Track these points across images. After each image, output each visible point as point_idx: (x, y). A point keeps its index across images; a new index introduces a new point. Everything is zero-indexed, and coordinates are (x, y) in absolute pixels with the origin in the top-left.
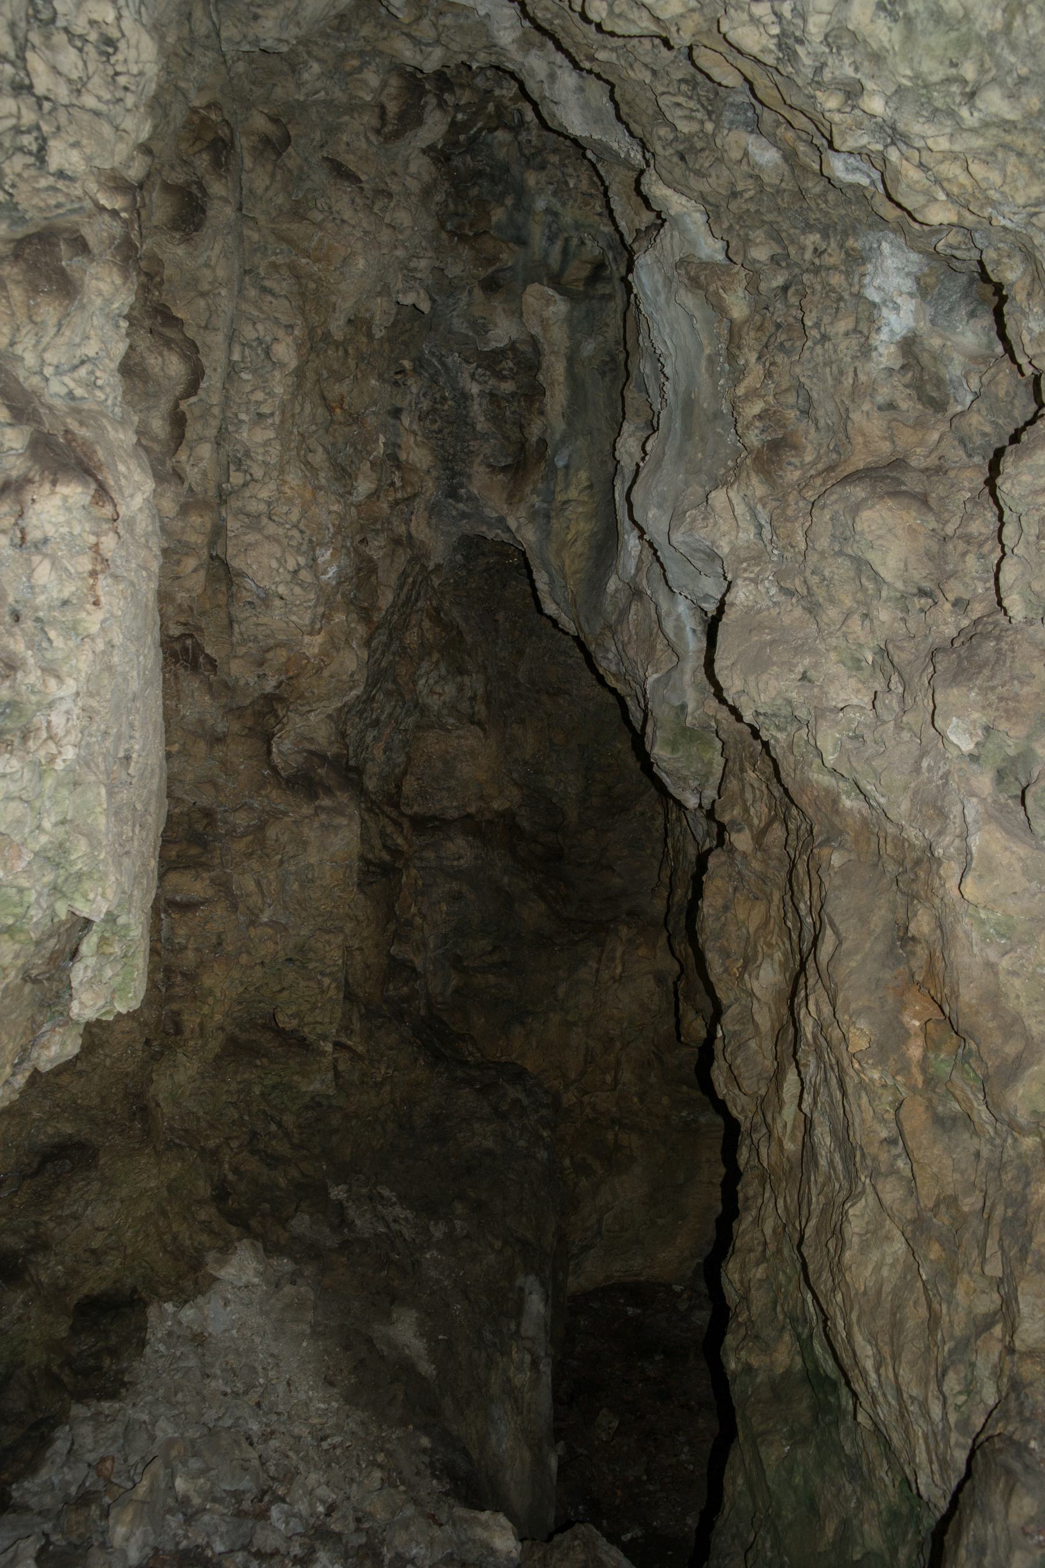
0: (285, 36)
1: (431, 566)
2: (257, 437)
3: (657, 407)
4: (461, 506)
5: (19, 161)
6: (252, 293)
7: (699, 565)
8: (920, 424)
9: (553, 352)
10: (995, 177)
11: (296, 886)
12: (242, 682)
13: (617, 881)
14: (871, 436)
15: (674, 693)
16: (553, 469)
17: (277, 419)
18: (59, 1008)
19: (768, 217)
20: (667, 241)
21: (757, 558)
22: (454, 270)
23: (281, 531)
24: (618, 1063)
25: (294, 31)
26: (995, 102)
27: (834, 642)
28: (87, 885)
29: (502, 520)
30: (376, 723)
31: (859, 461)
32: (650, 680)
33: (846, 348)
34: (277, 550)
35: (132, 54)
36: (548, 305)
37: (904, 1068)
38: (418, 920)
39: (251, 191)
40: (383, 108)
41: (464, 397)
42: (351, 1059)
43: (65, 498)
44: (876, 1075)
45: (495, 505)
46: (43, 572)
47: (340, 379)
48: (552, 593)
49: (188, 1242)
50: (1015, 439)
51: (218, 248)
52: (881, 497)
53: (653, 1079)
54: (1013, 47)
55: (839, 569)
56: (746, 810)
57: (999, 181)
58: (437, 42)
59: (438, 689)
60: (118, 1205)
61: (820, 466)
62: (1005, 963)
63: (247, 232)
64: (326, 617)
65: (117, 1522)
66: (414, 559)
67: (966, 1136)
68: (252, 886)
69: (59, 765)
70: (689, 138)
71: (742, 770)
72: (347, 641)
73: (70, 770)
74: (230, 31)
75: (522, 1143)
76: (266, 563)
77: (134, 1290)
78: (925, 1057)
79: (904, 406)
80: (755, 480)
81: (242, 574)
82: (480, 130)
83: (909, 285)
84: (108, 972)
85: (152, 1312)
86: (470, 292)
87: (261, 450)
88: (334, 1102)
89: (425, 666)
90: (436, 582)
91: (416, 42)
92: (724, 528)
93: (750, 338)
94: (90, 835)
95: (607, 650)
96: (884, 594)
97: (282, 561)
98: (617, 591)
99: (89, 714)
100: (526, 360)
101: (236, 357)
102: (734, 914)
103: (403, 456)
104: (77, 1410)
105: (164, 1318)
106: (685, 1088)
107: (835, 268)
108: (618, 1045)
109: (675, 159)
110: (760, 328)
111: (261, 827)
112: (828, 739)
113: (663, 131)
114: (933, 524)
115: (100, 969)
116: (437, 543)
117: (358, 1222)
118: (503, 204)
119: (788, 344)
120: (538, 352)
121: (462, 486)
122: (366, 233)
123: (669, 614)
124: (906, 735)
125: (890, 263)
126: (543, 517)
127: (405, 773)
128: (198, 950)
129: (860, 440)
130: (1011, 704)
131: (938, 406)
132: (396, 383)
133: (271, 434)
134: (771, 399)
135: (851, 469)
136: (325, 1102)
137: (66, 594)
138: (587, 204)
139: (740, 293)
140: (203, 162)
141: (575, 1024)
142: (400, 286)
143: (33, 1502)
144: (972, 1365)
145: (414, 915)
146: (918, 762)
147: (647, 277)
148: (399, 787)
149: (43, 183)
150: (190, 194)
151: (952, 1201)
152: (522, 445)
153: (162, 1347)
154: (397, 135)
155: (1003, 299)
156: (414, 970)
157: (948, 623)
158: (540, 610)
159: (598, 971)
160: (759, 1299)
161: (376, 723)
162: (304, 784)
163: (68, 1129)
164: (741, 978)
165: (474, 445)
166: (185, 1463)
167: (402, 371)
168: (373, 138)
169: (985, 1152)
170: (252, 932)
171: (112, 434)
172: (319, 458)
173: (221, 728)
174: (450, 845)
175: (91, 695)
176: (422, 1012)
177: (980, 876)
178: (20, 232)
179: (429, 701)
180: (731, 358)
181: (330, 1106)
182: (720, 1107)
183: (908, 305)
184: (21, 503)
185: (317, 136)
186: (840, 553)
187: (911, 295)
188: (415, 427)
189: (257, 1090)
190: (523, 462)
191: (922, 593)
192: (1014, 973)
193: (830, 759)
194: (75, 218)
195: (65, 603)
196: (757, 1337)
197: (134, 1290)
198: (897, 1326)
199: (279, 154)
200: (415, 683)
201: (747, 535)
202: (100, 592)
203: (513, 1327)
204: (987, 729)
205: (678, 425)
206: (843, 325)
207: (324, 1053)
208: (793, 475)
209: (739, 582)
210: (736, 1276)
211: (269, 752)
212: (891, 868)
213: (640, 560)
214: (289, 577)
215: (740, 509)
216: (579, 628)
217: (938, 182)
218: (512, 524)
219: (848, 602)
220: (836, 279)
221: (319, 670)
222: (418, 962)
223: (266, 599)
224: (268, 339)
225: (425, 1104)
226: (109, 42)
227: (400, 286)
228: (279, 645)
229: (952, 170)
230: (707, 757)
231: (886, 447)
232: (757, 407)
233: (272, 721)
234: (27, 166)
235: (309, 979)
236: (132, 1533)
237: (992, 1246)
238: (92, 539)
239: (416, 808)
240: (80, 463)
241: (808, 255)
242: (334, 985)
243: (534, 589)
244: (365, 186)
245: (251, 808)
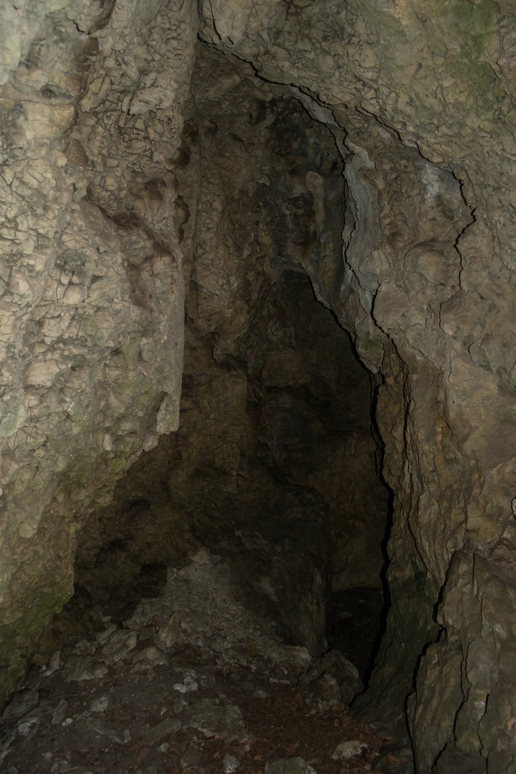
0: (217, 96)
1: (272, 283)
2: (208, 236)
3: (355, 220)
4: (283, 259)
5: (145, 159)
6: (205, 184)
7: (370, 278)
8: (444, 225)
9: (318, 198)
10: (450, 150)
11: (223, 406)
12: (202, 328)
14: (426, 230)
15: (364, 327)
16: (320, 244)
17: (215, 229)
18: (152, 429)
19: (388, 155)
20: (355, 161)
21: (389, 275)
22: (279, 168)
23: (217, 270)
25: (220, 94)
26: (444, 129)
27: (413, 302)
28: (167, 381)
29: (300, 264)
30: (251, 347)
31: (422, 239)
32: (357, 323)
33: (417, 200)
34: (215, 277)
35: (176, 122)
36: (315, 179)
37: (435, 444)
38: (269, 427)
39: (204, 148)
40: (251, 115)
41: (284, 216)
43: (164, 261)
44: (427, 448)
45: (297, 258)
46: (158, 283)
47: (237, 213)
48: (320, 292)
49: (181, 546)
50: (463, 232)
51: (194, 170)
52: (426, 252)
54: (447, 116)
55: (414, 277)
56: (391, 369)
57: (451, 151)
58: (271, 91)
59: (276, 333)
60: (157, 526)
61: (409, 241)
62: (464, 404)
63: (203, 162)
64: (233, 302)
65: (162, 633)
66: (265, 281)
67: (456, 465)
68: (207, 405)
69: (162, 341)
70: (360, 128)
71: (390, 354)
72: (241, 312)
73: (164, 343)
74: (198, 96)
75: (312, 516)
76: (210, 283)
77: (162, 562)
78: (442, 440)
79: (438, 219)
80: (387, 247)
81: (202, 287)
82: (287, 114)
83: (436, 178)
84: (168, 417)
85: (169, 570)
86: (285, 176)
87: (209, 241)
89: (270, 324)
90: (274, 290)
91: (263, 92)
92: (378, 264)
93: (385, 196)
94: (170, 364)
95: (342, 314)
96: (429, 285)
97: (217, 282)
98: (345, 290)
99: (170, 326)
100: (308, 201)
101: (200, 208)
102: (388, 408)
103: (260, 240)
104: (144, 600)
105: (172, 574)
107: (411, 172)
108: (354, 484)
109: (356, 135)
110: (388, 192)
111: (210, 381)
112: (410, 336)
113: (350, 126)
114: (444, 261)
115: (165, 415)
116: (274, 273)
117: (247, 544)
118: (297, 141)
119: (397, 198)
120: (312, 197)
121: (284, 251)
122: (246, 160)
123: (362, 298)
124: (435, 332)
125: (429, 171)
126: (316, 263)
127: (263, 367)
128: (187, 428)
129: (422, 232)
130: (464, 319)
131: (451, 218)
132: (257, 212)
133: (213, 235)
134: (392, 218)
135: (418, 242)
137: (164, 290)
138: (329, 140)
139: (382, 180)
140: (188, 140)
142: (258, 176)
143: (131, 627)
144: (456, 538)
146: (437, 340)
147: (350, 173)
148: (261, 373)
149: (152, 165)
150: (185, 152)
151: (451, 486)
152: (307, 233)
153: (173, 583)
154: (256, 123)
155: (462, 185)
156: (268, 446)
157: (449, 293)
158: (316, 299)
159: (344, 451)
160: (399, 552)
161: (251, 347)
162: (226, 365)
163: (140, 494)
164: (391, 432)
165: (288, 235)
166: (184, 619)
167: (259, 207)
168: (248, 125)
169: (461, 470)
170: (207, 421)
171: (173, 241)
172: (230, 243)
173: (195, 345)
175: (170, 321)
176: (271, 465)
177: (455, 375)
178: (146, 180)
180: (379, 203)
182: (386, 485)
183: (436, 185)
184: (152, 263)
185: (227, 126)
186: (414, 272)
187: (437, 181)
188: (265, 228)
189: (207, 490)
190: (308, 241)
191: (441, 284)
192: (467, 407)
193: (411, 342)
194: (161, 175)
195: (164, 292)
196: (398, 566)
197: (162, 562)
198: (435, 532)
199: (214, 134)
200: (266, 330)
201: (386, 266)
202: (174, 289)
203: (309, 587)
204: (458, 328)
205: (362, 227)
206: (415, 192)
207: (233, 476)
208: (400, 245)
209: (383, 283)
210: (391, 546)
211: (213, 354)
212: (432, 378)
213: (352, 278)
214: (220, 287)
215: (383, 257)
216: (331, 306)
217: (434, 150)
218: (304, 265)
219: (418, 288)
220: (412, 176)
221: (231, 322)
222: (269, 444)
223: (211, 296)
224: (211, 200)
226: (169, 119)
227: (258, 176)
228: (216, 313)
229: (437, 147)
230: (379, 352)
231: (431, 234)
232: (388, 221)
233: (214, 342)
234: (147, 161)
236: (168, 636)
237: (461, 497)
238: (171, 273)
239: (267, 383)
240: (167, 250)
241: (402, 168)
243: (314, 291)
244: (245, 142)
245: (206, 375)
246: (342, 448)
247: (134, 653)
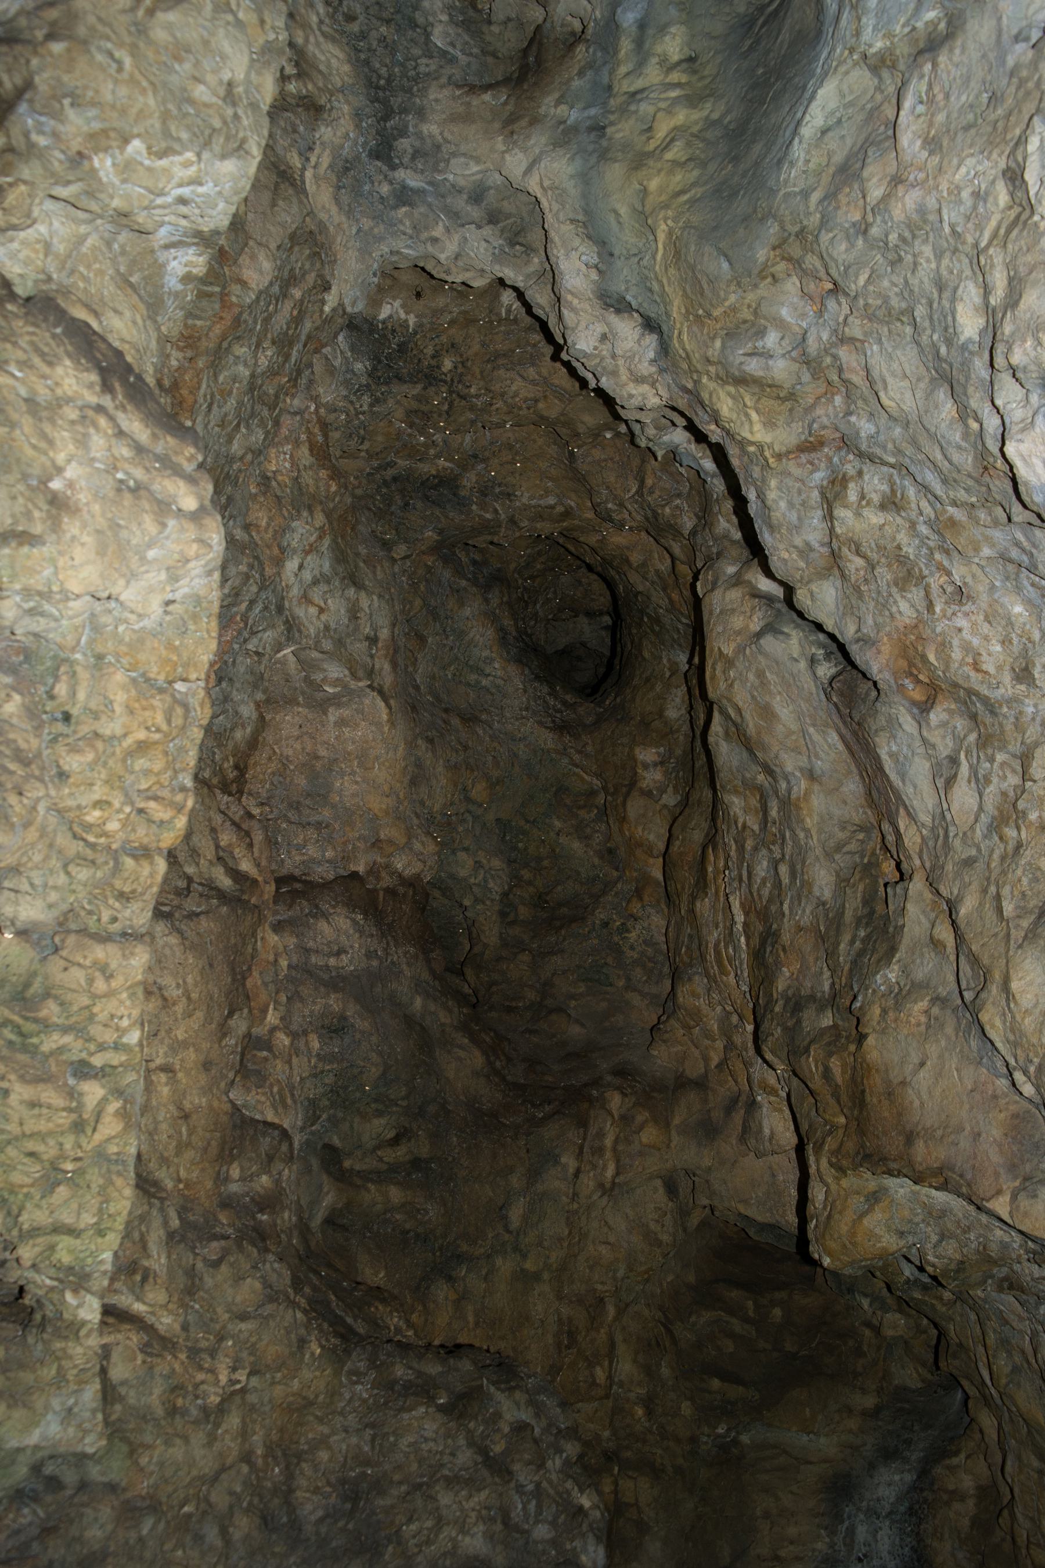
13: (575, 1030)
24: (612, 1345)
38: (283, 1040)
42: (145, 1348)
53: (665, 1371)
88: (95, 1473)
106: (716, 1383)
108: (611, 1311)
136: (70, 1477)
141: (536, 1277)
145: (273, 1030)
174: (322, 925)
179: (300, 612)
181: (83, 1485)
207: (74, 1329)
225: (324, 1455)
235: (38, 1080)
242: (115, 1105)
246: (569, 1161)
247: (575, 301)
